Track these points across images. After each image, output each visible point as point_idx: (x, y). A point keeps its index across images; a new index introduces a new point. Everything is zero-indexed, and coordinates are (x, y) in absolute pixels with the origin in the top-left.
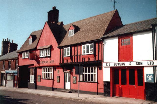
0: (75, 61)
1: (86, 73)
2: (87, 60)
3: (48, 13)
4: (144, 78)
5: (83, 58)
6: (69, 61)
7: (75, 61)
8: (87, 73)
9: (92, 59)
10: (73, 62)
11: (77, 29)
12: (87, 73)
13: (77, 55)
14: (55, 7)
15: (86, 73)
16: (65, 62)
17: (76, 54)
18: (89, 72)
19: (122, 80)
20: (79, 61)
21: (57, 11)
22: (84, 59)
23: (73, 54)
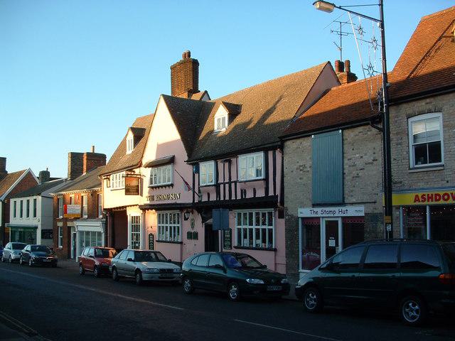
0: (224, 197)
1: (251, 227)
2: (250, 195)
3: (173, 68)
4: (287, 77)
5: (242, 191)
6: (213, 198)
7: (224, 197)
8: (254, 227)
9: (261, 193)
10: (222, 199)
11: (234, 110)
12: (254, 227)
13: (230, 183)
14: (189, 53)
15: (251, 227)
16: (205, 199)
17: (227, 180)
18: (258, 224)
19: (319, 242)
20: (233, 198)
21: (195, 64)
22: (244, 192)
23: (221, 181)
